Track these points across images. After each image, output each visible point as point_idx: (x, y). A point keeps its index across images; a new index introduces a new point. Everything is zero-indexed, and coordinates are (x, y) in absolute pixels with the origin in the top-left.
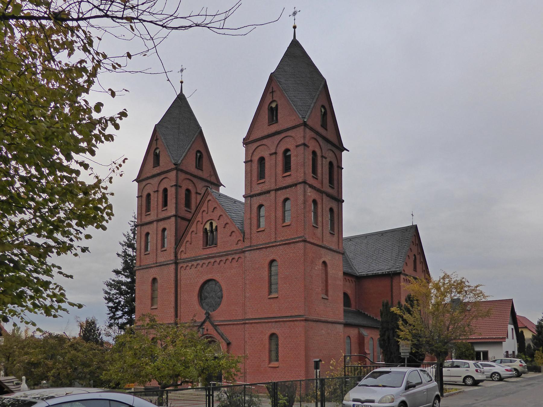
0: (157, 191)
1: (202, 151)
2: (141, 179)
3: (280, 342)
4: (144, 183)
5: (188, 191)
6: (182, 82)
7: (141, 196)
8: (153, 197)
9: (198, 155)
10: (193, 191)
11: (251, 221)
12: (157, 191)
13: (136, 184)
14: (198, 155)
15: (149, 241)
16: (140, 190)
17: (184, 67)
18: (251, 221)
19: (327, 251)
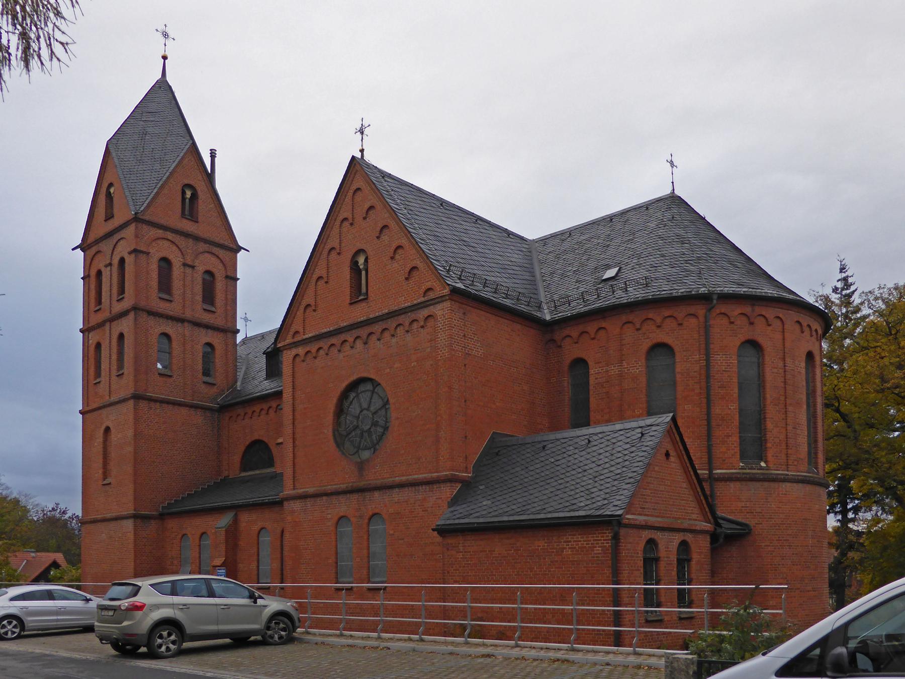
0: (110, 264)
1: (199, 190)
2: (89, 241)
3: (767, 359)
4: (93, 250)
5: (165, 262)
6: (165, 58)
7: (89, 276)
8: (106, 273)
9: (188, 194)
10: (177, 261)
11: (189, 322)
12: (110, 264)
13: (80, 254)
14: (188, 194)
15: (409, 304)
16: (88, 264)
17: (161, 28)
18: (189, 322)
19: (109, 409)
